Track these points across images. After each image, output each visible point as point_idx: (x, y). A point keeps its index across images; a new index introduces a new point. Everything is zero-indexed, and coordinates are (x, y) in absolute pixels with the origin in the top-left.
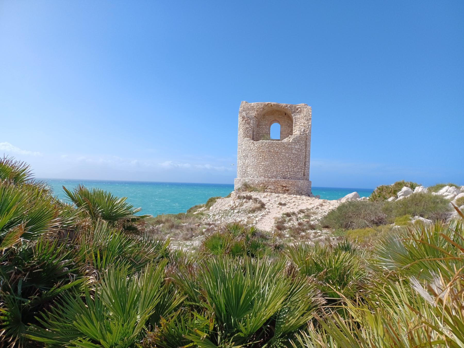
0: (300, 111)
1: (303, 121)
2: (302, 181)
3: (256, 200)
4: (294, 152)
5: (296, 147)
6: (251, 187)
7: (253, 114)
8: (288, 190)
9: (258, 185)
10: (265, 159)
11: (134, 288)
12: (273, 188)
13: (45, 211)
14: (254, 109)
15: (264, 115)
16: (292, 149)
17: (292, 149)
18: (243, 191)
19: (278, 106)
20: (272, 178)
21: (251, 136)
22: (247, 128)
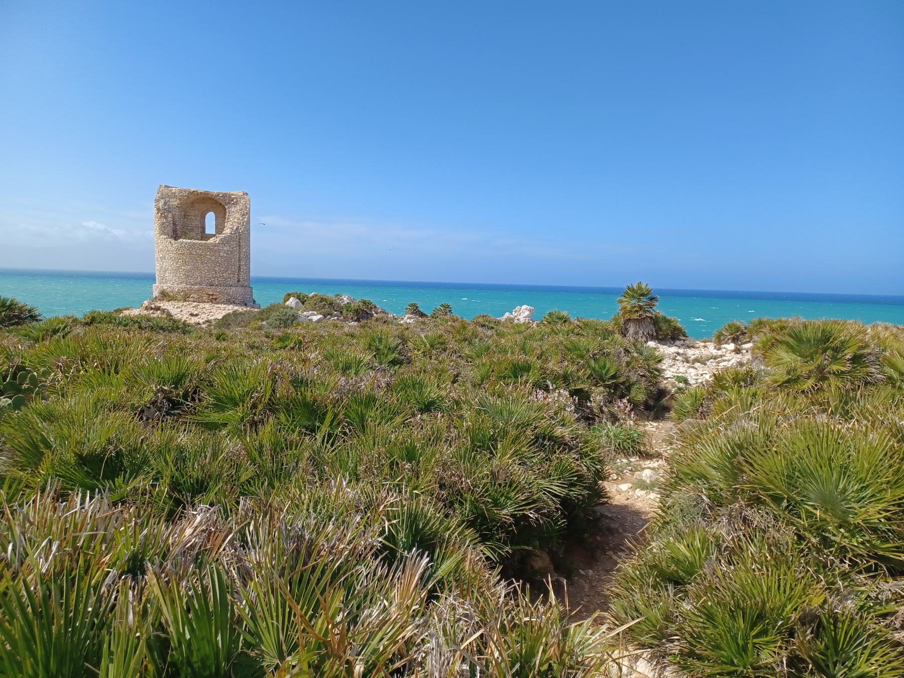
0: (236, 203)
1: (237, 215)
2: (234, 289)
3: (163, 311)
4: (222, 254)
5: (225, 249)
6: (169, 296)
7: (175, 202)
8: (216, 299)
9: (179, 292)
10: (185, 263)
11: (211, 603)
12: (196, 296)
13: (701, 625)
14: (175, 196)
15: (192, 203)
16: (219, 251)
17: (219, 251)
18: (160, 300)
19: (206, 193)
20: (196, 284)
21: (171, 233)
22: (163, 223)
